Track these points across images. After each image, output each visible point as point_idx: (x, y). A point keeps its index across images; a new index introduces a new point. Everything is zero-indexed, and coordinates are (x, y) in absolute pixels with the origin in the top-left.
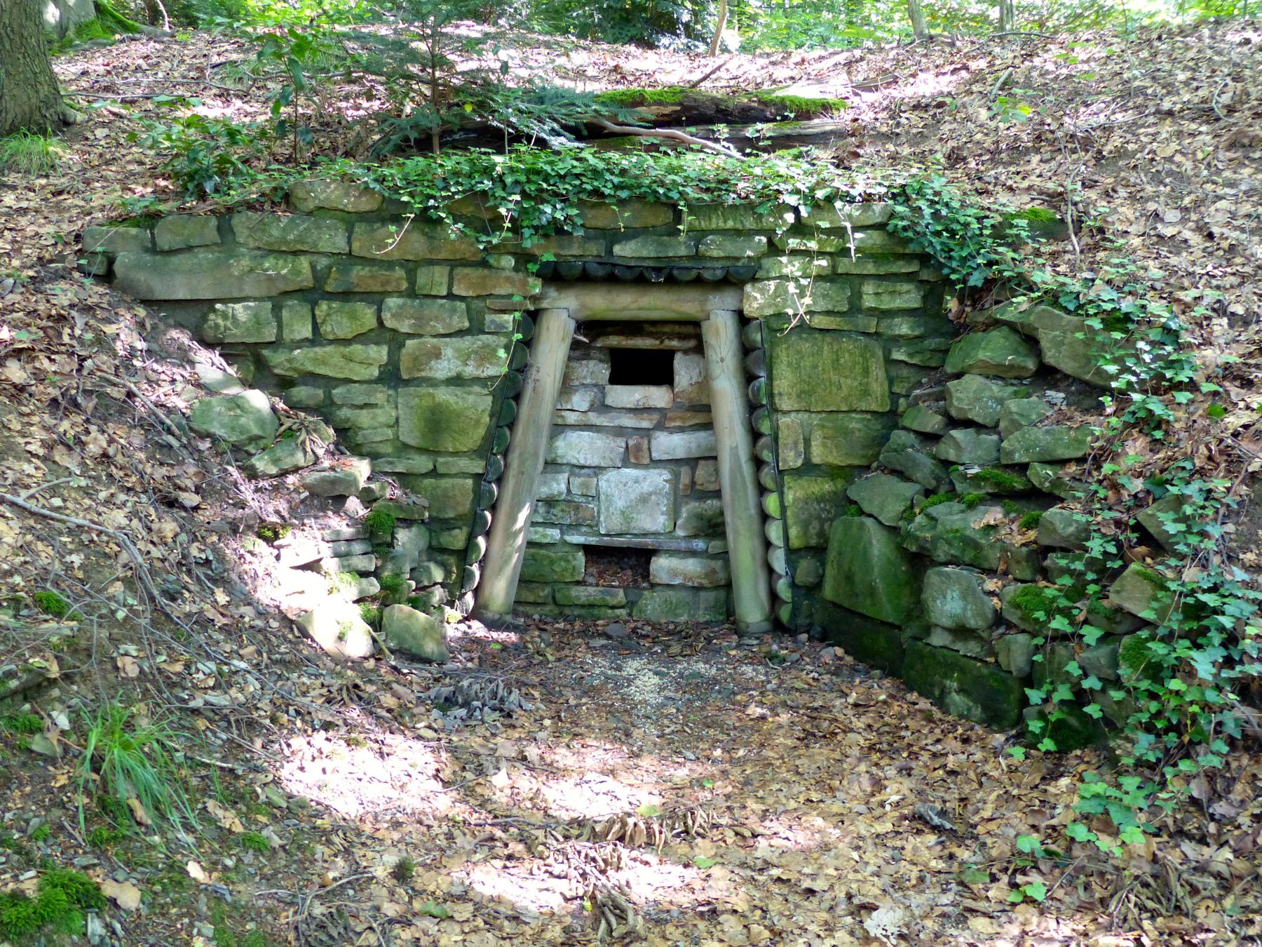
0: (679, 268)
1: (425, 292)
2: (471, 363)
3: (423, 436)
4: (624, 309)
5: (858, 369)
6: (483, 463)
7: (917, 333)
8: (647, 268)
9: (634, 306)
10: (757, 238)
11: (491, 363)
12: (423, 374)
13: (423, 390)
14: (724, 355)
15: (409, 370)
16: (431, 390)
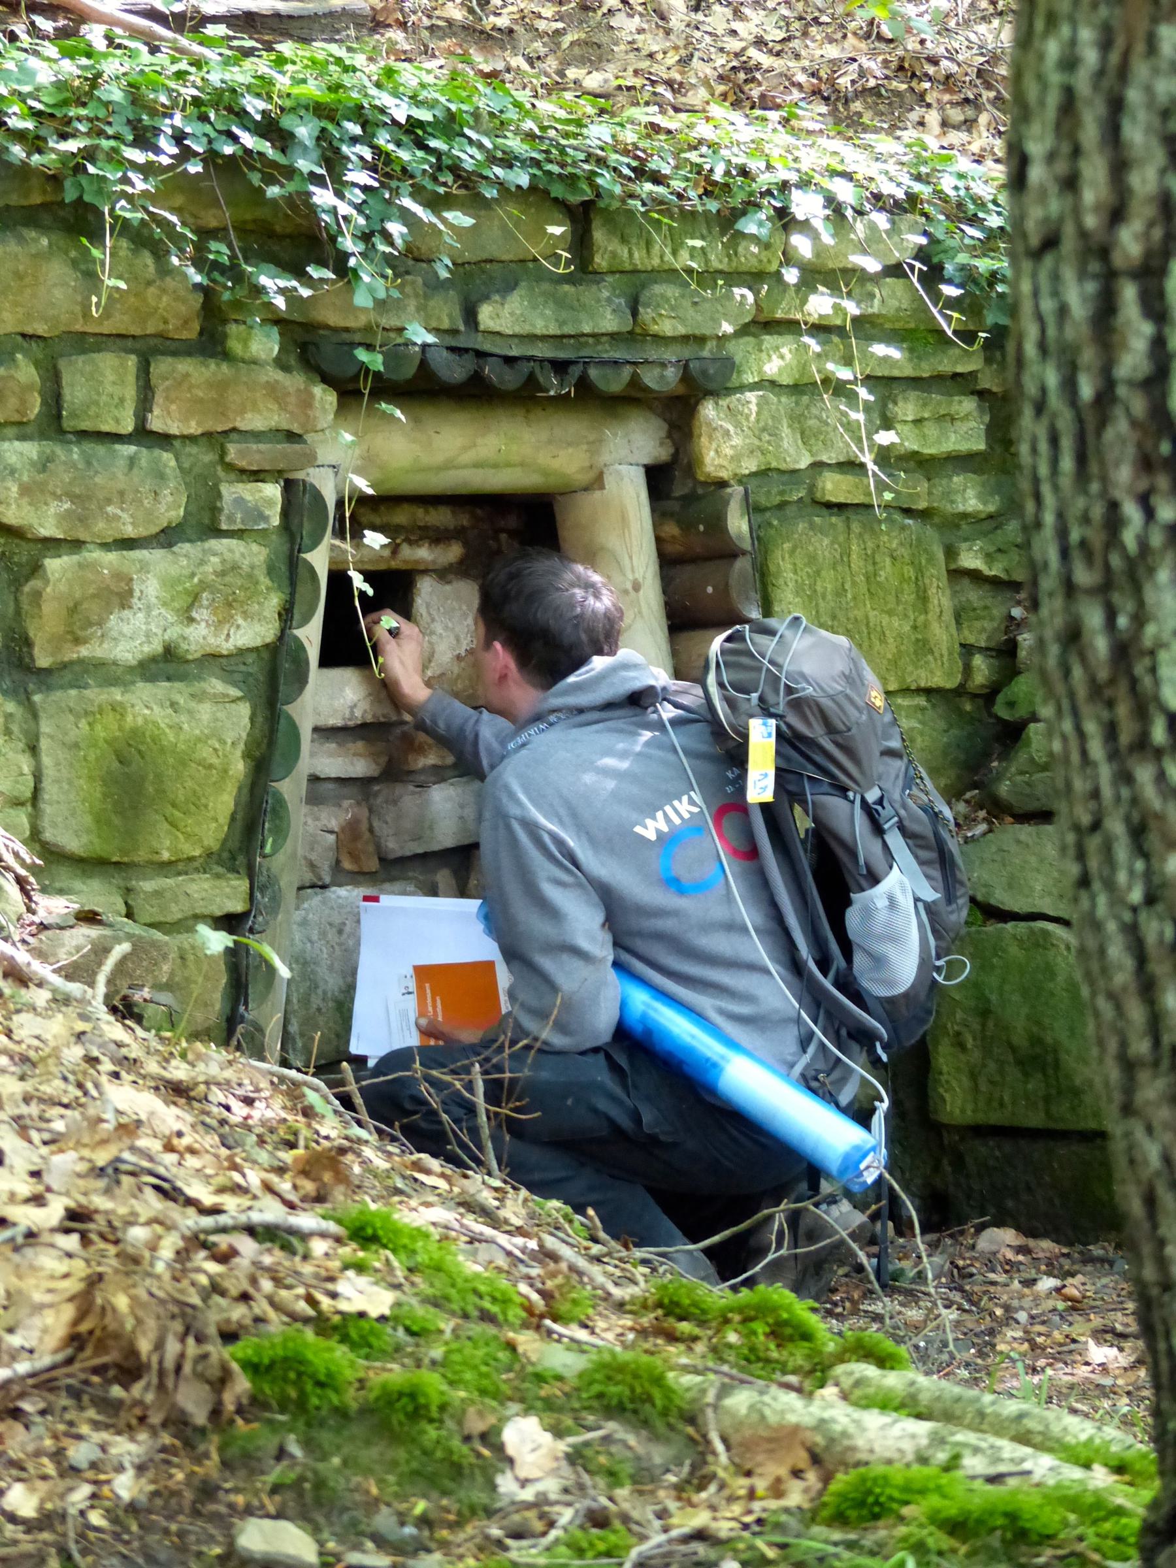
0: (603, 363)
1: (85, 425)
2: (199, 614)
3: (100, 820)
4: (448, 465)
5: (909, 597)
6: (243, 885)
7: (991, 508)
8: (542, 361)
9: (468, 457)
10: (737, 291)
11: (246, 615)
12: (84, 651)
13: (97, 695)
14: (639, 576)
15: (56, 642)
16: (117, 695)
